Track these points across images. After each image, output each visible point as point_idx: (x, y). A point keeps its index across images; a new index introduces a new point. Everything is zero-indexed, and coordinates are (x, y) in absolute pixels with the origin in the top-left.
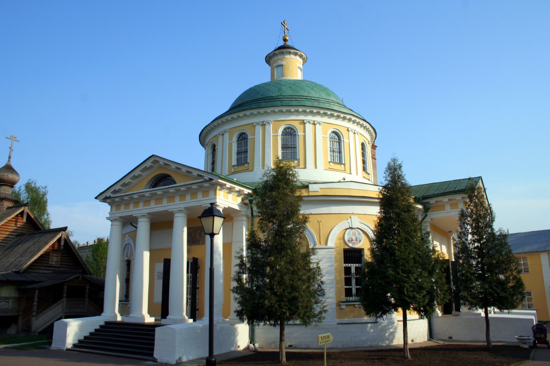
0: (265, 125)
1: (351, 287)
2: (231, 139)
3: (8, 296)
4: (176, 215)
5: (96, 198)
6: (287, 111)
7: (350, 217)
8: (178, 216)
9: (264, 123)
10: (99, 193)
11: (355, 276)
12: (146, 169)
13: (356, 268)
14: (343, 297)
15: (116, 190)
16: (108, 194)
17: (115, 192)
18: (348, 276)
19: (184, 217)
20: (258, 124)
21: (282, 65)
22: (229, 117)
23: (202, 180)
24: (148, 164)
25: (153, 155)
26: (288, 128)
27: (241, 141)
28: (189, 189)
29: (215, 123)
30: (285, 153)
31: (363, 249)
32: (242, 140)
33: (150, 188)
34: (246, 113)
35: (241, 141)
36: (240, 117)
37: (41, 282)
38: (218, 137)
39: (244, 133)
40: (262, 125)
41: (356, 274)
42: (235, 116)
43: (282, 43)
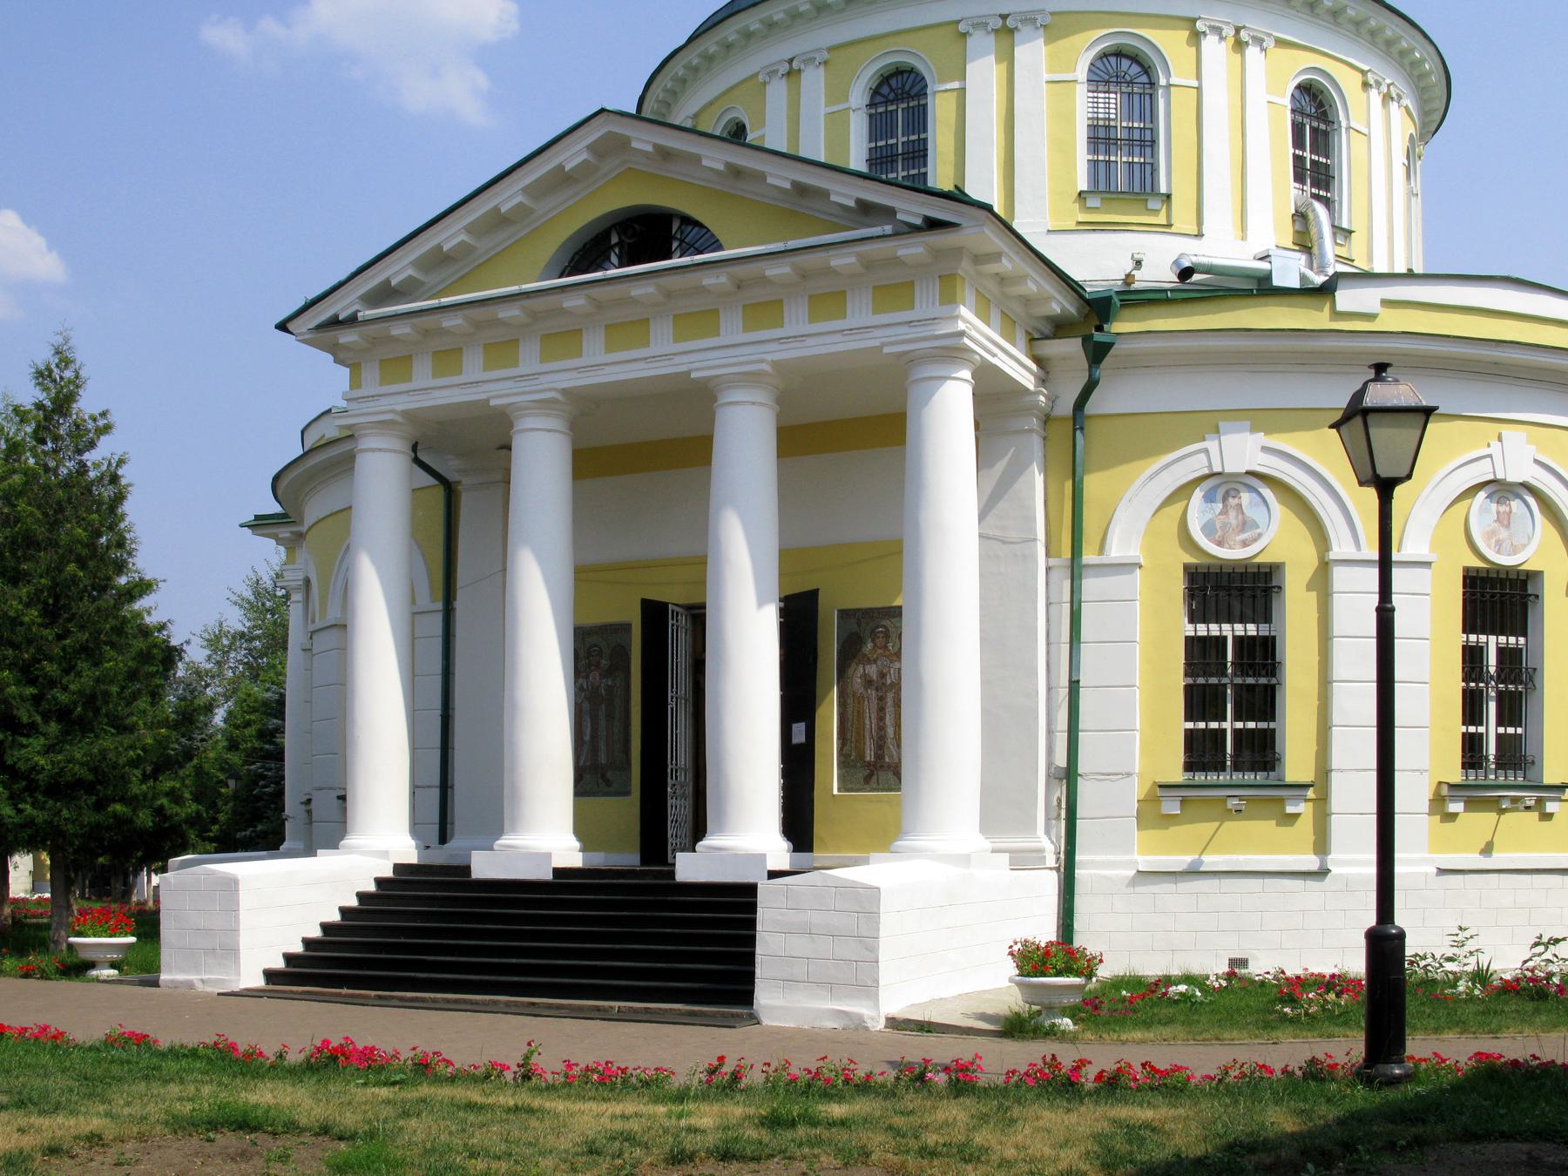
0: (1011, 32)
1: (1501, 730)
2: (837, 93)
3: (1377, 570)
5: (283, 326)
7: (1500, 439)
9: (1010, 23)
10: (301, 303)
12: (561, 179)
13: (1502, 652)
14: (1456, 776)
15: (394, 283)
16: (341, 306)
17: (385, 293)
20: (981, 25)
23: (888, 229)
24: (572, 156)
25: (602, 110)
27: (894, 107)
28: (804, 275)
30: (1102, 167)
31: (1536, 576)
32: (896, 100)
33: (560, 277)
35: (894, 107)
37: (1433, 489)
38: (765, 84)
40: (996, 31)
41: (1500, 679)
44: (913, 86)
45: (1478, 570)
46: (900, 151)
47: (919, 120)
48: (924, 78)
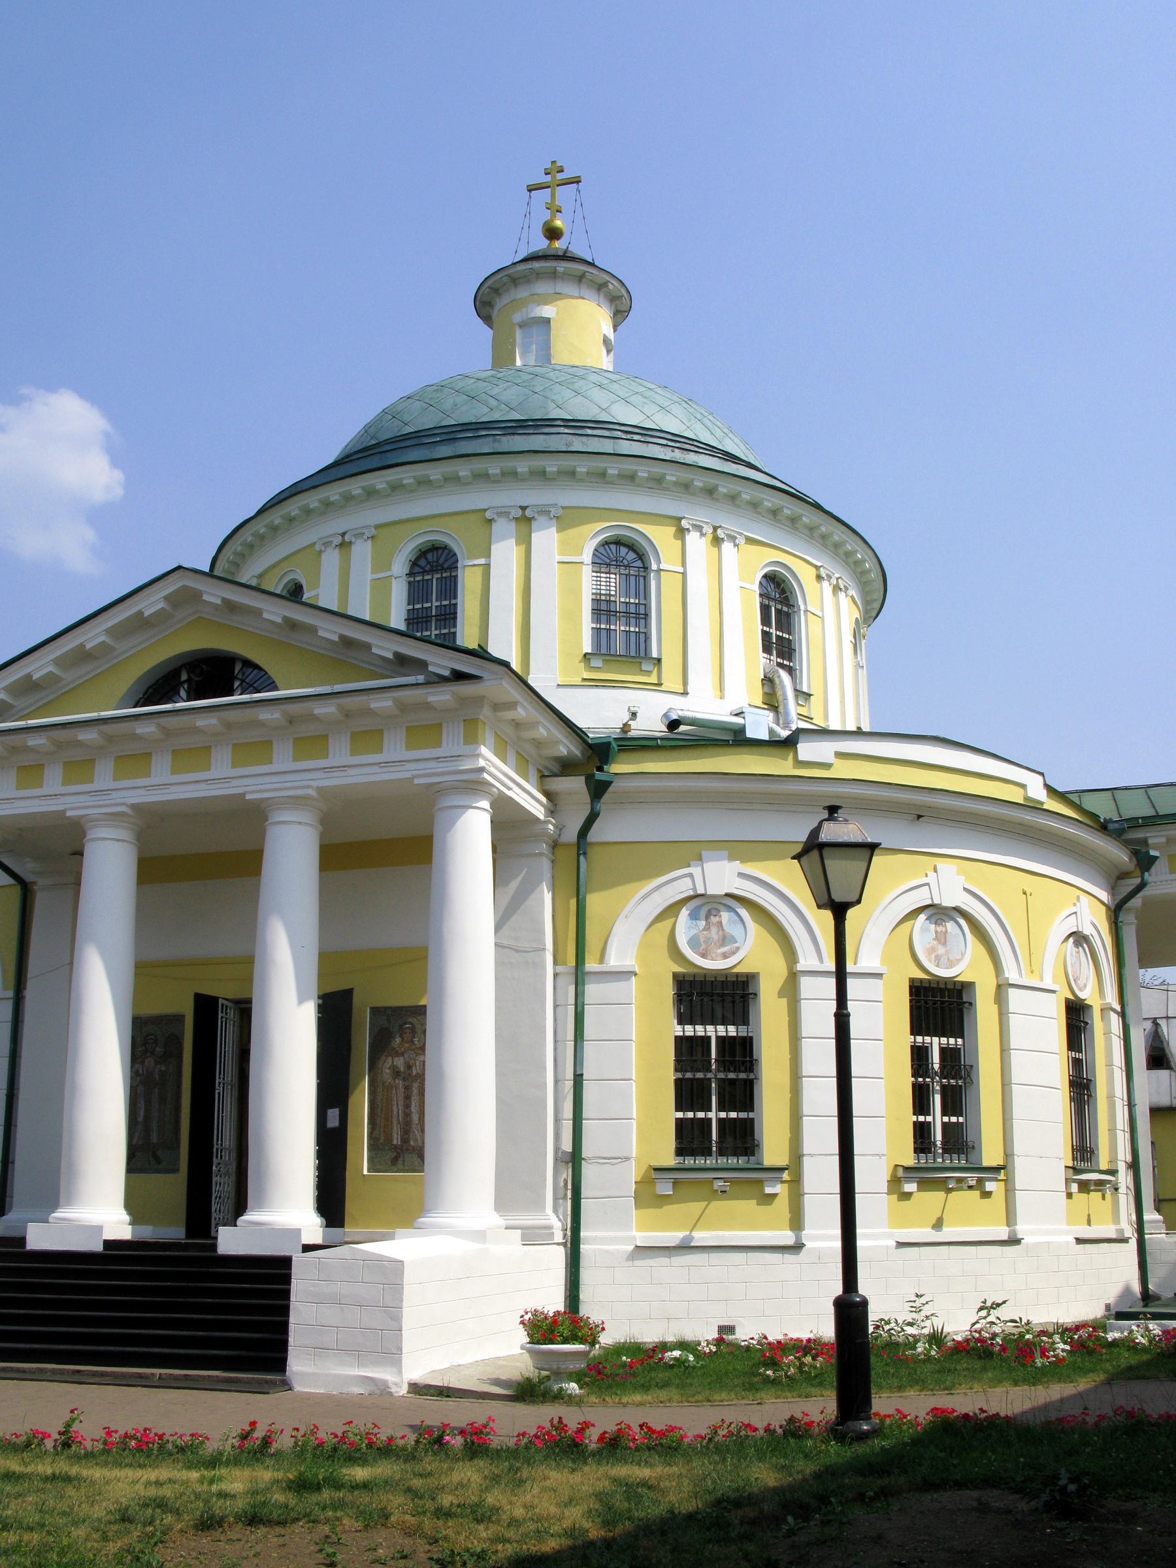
0: (529, 520)
1: (946, 1119)
2: (382, 563)
4: (92, 834)
6: (621, 476)
7: (935, 870)
8: (285, 819)
9: (528, 513)
11: (709, 1075)
12: (140, 623)
14: (909, 1160)
18: (689, 1075)
19: (130, 843)
20: (504, 514)
21: (547, 321)
22: (333, 492)
23: (421, 678)
24: (151, 604)
25: (179, 567)
29: (275, 517)
34: (287, 510)
35: (429, 577)
36: (332, 503)
38: (320, 552)
39: (445, 548)
42: (355, 486)
43: (540, 243)
44: (446, 560)
45: (921, 980)
46: (434, 614)
47: (450, 588)
48: (455, 554)
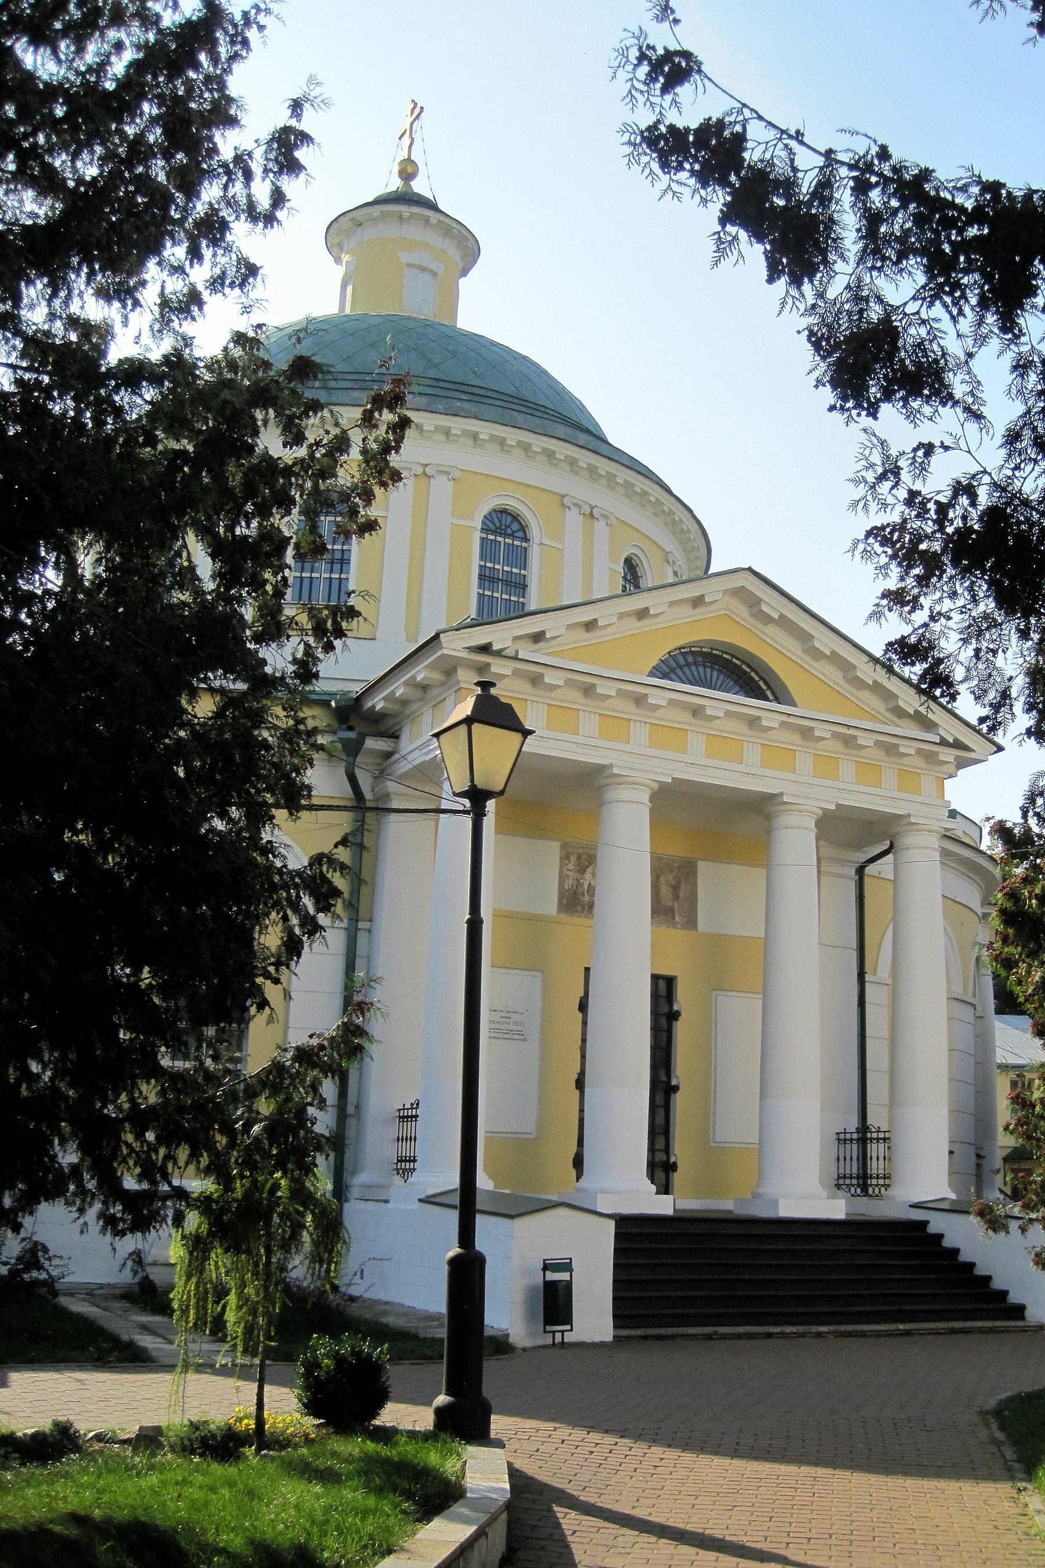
26: (504, 512)
43: (395, 184)
47: (521, 558)
